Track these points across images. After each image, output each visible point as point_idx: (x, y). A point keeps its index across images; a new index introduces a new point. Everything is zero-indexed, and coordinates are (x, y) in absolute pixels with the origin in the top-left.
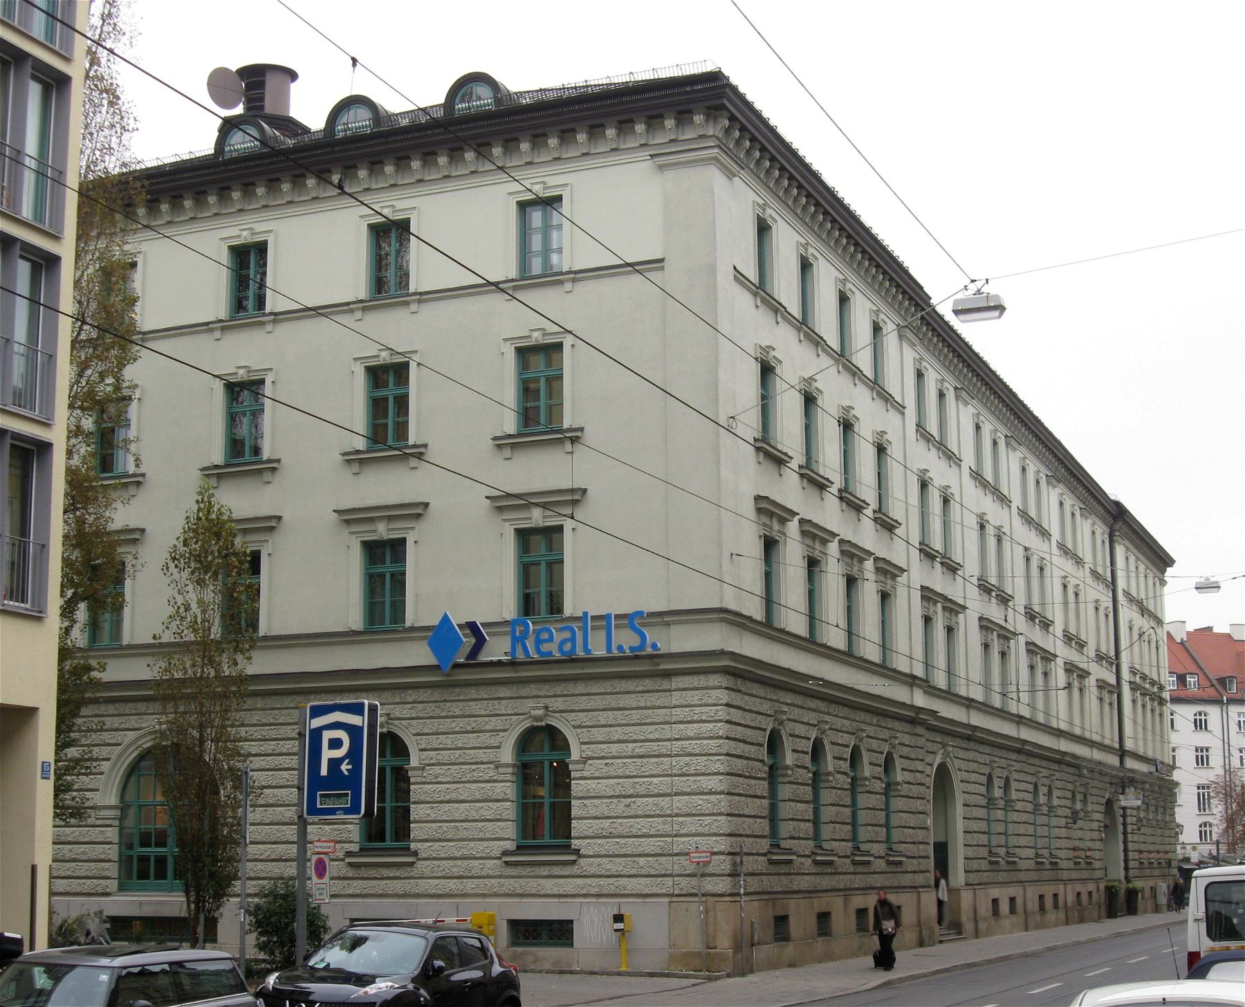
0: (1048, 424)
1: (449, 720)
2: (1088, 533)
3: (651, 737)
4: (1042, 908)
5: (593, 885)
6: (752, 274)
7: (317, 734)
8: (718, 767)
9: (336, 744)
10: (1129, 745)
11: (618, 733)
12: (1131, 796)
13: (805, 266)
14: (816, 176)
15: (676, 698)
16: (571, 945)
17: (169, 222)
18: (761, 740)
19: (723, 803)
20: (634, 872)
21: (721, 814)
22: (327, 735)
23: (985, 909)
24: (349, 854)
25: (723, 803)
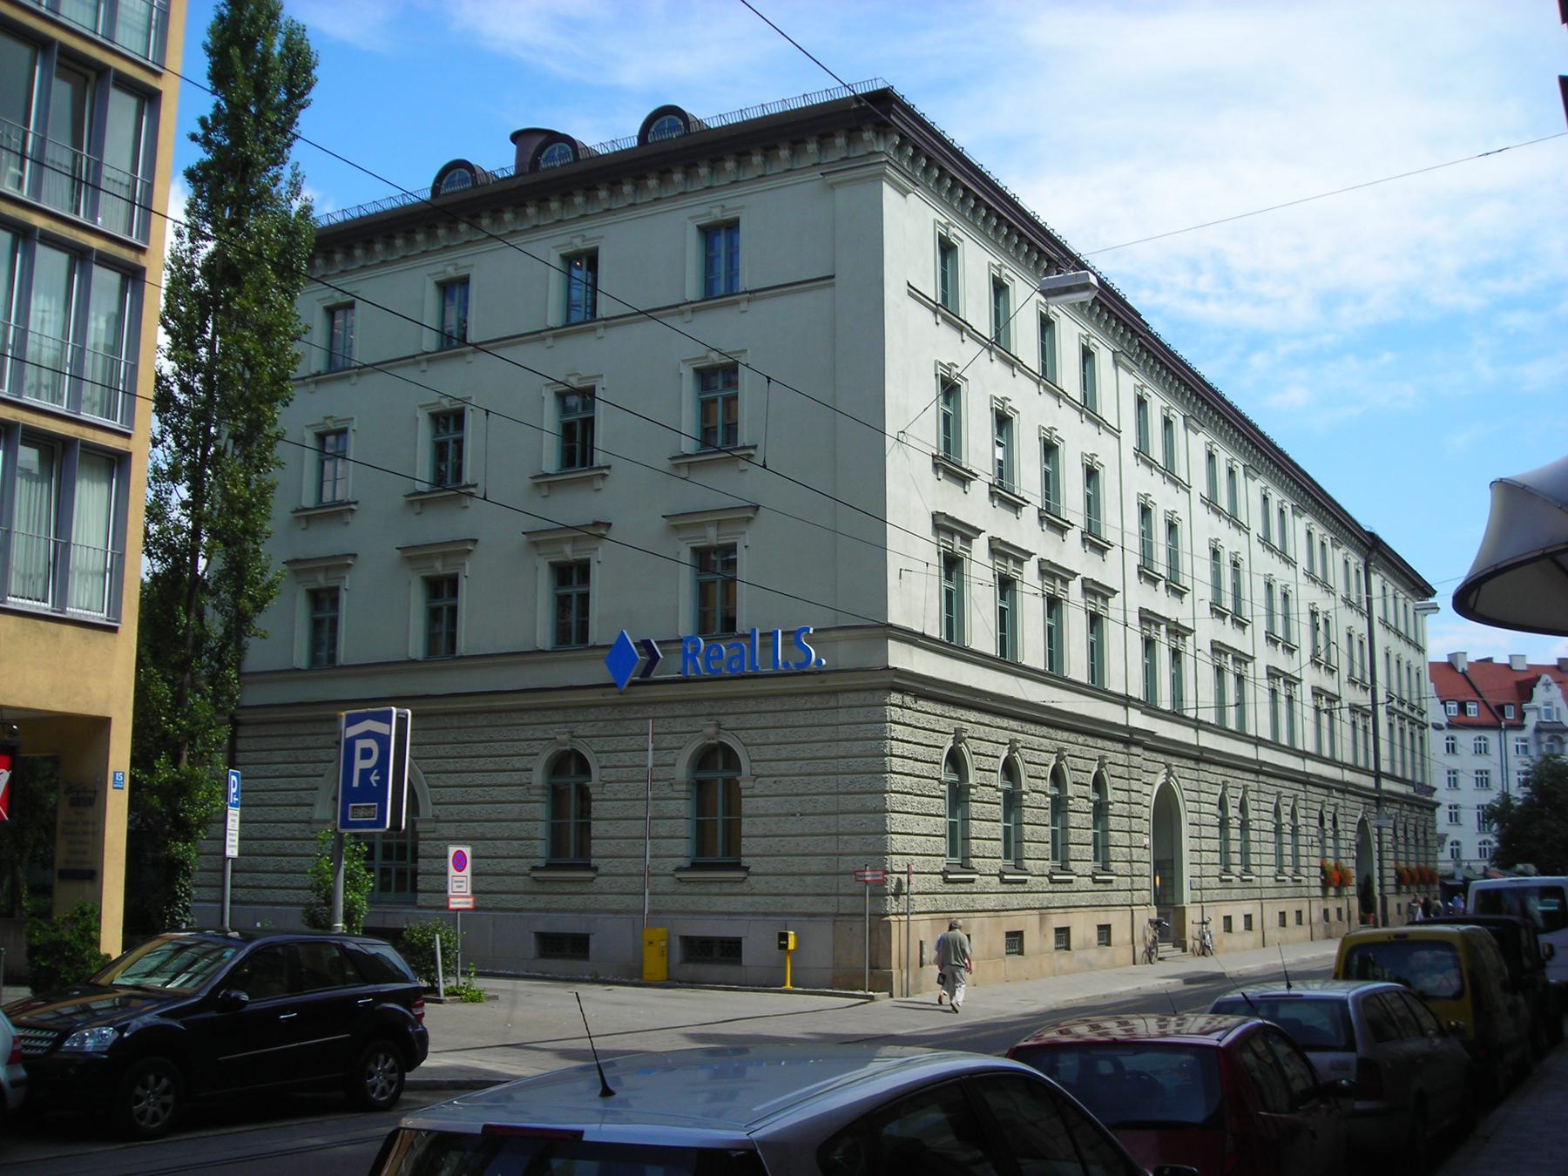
2: (1341, 560)
4: (1283, 923)
5: (762, 903)
6: (931, 290)
7: (350, 744)
9: (367, 754)
10: (1385, 767)
11: (785, 751)
13: (999, 288)
15: (842, 716)
16: (739, 962)
17: (383, 262)
18: (935, 758)
22: (361, 744)
23: (1216, 926)
24: (535, 868)
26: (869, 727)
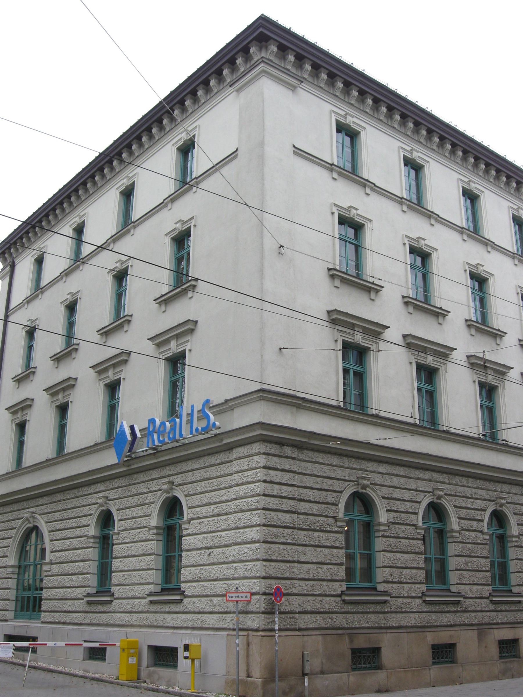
1: (131, 498)
3: (223, 499)
8: (256, 520)
15: (235, 466)
19: (259, 550)
20: (210, 610)
21: (257, 560)
25: (259, 550)
26: (250, 473)
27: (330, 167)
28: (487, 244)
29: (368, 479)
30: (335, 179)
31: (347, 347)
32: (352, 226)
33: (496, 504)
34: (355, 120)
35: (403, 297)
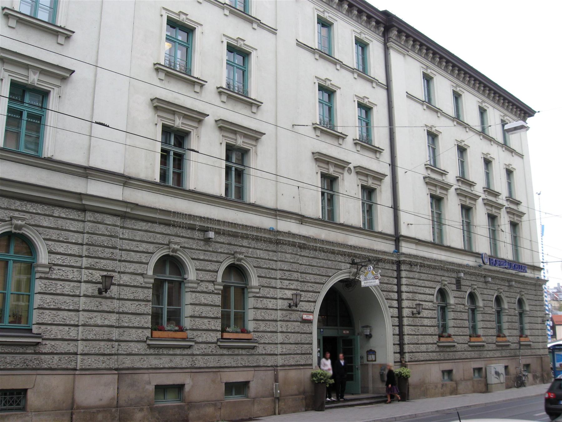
0: (498, 84)
10: (404, 231)
12: (370, 276)
14: (531, 108)
27: (312, 50)
28: (437, 111)
29: (23, 219)
30: (316, 59)
31: (167, 131)
32: (327, 91)
33: (234, 258)
34: (330, 15)
35: (354, 140)
